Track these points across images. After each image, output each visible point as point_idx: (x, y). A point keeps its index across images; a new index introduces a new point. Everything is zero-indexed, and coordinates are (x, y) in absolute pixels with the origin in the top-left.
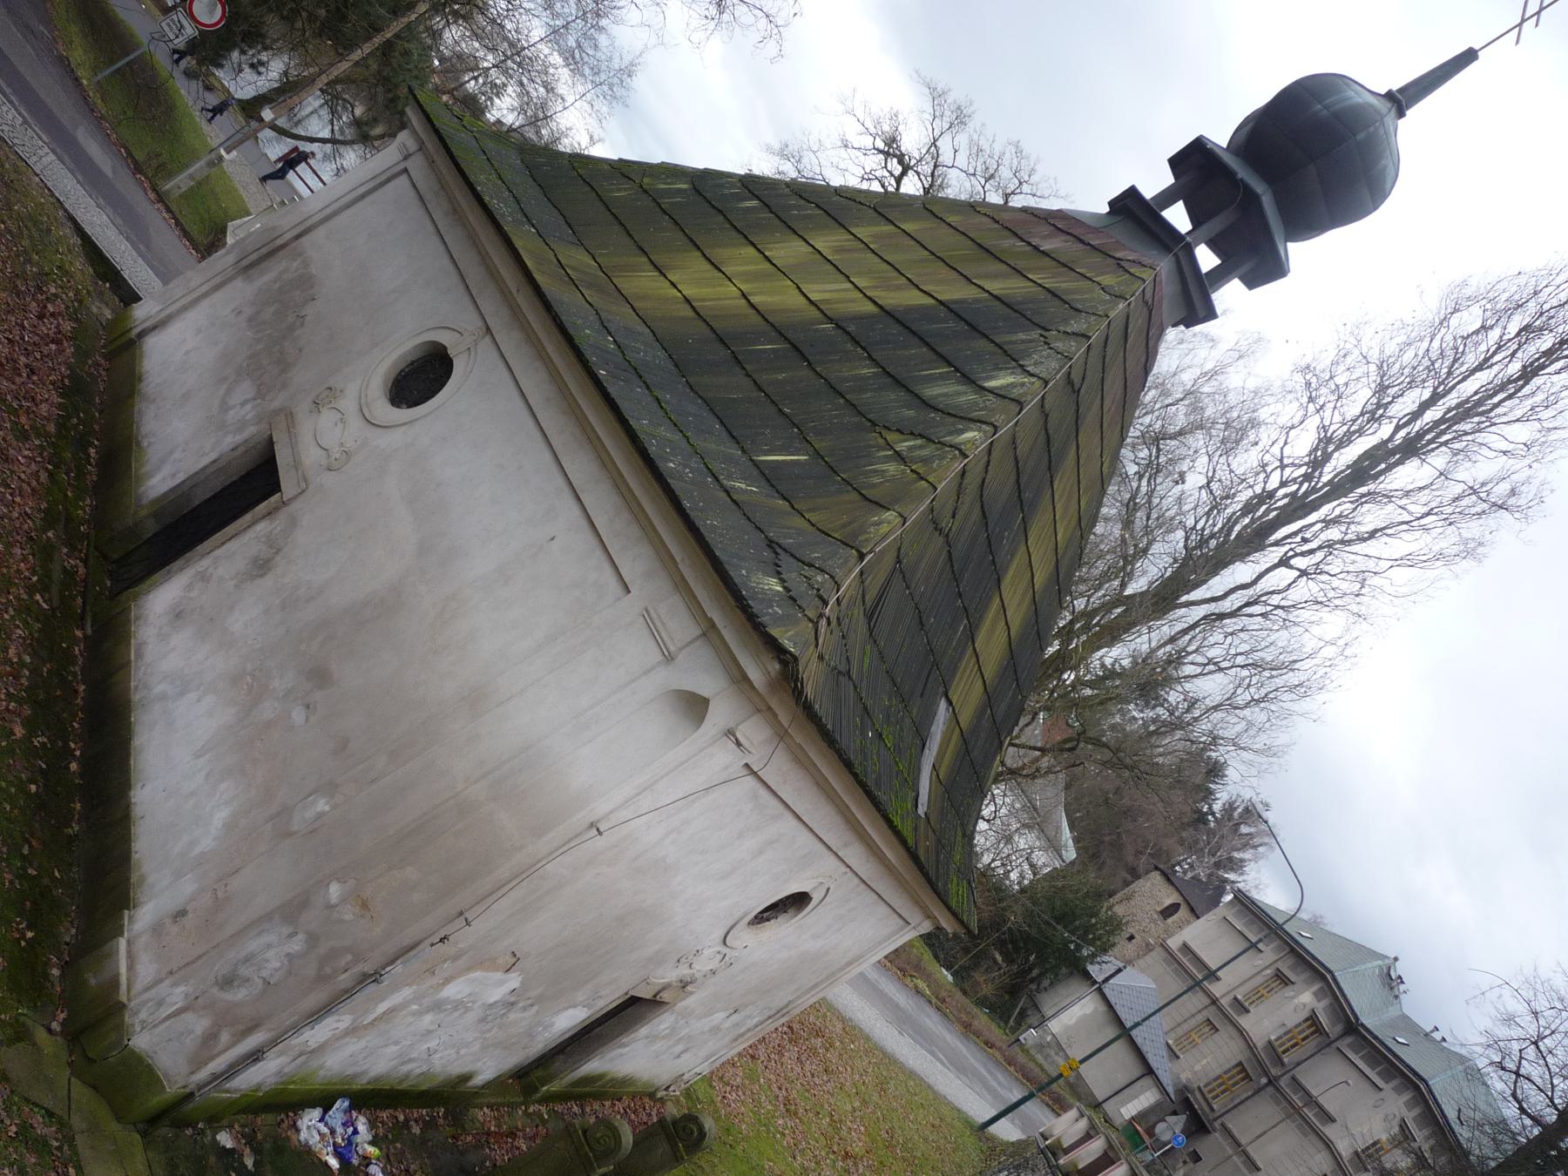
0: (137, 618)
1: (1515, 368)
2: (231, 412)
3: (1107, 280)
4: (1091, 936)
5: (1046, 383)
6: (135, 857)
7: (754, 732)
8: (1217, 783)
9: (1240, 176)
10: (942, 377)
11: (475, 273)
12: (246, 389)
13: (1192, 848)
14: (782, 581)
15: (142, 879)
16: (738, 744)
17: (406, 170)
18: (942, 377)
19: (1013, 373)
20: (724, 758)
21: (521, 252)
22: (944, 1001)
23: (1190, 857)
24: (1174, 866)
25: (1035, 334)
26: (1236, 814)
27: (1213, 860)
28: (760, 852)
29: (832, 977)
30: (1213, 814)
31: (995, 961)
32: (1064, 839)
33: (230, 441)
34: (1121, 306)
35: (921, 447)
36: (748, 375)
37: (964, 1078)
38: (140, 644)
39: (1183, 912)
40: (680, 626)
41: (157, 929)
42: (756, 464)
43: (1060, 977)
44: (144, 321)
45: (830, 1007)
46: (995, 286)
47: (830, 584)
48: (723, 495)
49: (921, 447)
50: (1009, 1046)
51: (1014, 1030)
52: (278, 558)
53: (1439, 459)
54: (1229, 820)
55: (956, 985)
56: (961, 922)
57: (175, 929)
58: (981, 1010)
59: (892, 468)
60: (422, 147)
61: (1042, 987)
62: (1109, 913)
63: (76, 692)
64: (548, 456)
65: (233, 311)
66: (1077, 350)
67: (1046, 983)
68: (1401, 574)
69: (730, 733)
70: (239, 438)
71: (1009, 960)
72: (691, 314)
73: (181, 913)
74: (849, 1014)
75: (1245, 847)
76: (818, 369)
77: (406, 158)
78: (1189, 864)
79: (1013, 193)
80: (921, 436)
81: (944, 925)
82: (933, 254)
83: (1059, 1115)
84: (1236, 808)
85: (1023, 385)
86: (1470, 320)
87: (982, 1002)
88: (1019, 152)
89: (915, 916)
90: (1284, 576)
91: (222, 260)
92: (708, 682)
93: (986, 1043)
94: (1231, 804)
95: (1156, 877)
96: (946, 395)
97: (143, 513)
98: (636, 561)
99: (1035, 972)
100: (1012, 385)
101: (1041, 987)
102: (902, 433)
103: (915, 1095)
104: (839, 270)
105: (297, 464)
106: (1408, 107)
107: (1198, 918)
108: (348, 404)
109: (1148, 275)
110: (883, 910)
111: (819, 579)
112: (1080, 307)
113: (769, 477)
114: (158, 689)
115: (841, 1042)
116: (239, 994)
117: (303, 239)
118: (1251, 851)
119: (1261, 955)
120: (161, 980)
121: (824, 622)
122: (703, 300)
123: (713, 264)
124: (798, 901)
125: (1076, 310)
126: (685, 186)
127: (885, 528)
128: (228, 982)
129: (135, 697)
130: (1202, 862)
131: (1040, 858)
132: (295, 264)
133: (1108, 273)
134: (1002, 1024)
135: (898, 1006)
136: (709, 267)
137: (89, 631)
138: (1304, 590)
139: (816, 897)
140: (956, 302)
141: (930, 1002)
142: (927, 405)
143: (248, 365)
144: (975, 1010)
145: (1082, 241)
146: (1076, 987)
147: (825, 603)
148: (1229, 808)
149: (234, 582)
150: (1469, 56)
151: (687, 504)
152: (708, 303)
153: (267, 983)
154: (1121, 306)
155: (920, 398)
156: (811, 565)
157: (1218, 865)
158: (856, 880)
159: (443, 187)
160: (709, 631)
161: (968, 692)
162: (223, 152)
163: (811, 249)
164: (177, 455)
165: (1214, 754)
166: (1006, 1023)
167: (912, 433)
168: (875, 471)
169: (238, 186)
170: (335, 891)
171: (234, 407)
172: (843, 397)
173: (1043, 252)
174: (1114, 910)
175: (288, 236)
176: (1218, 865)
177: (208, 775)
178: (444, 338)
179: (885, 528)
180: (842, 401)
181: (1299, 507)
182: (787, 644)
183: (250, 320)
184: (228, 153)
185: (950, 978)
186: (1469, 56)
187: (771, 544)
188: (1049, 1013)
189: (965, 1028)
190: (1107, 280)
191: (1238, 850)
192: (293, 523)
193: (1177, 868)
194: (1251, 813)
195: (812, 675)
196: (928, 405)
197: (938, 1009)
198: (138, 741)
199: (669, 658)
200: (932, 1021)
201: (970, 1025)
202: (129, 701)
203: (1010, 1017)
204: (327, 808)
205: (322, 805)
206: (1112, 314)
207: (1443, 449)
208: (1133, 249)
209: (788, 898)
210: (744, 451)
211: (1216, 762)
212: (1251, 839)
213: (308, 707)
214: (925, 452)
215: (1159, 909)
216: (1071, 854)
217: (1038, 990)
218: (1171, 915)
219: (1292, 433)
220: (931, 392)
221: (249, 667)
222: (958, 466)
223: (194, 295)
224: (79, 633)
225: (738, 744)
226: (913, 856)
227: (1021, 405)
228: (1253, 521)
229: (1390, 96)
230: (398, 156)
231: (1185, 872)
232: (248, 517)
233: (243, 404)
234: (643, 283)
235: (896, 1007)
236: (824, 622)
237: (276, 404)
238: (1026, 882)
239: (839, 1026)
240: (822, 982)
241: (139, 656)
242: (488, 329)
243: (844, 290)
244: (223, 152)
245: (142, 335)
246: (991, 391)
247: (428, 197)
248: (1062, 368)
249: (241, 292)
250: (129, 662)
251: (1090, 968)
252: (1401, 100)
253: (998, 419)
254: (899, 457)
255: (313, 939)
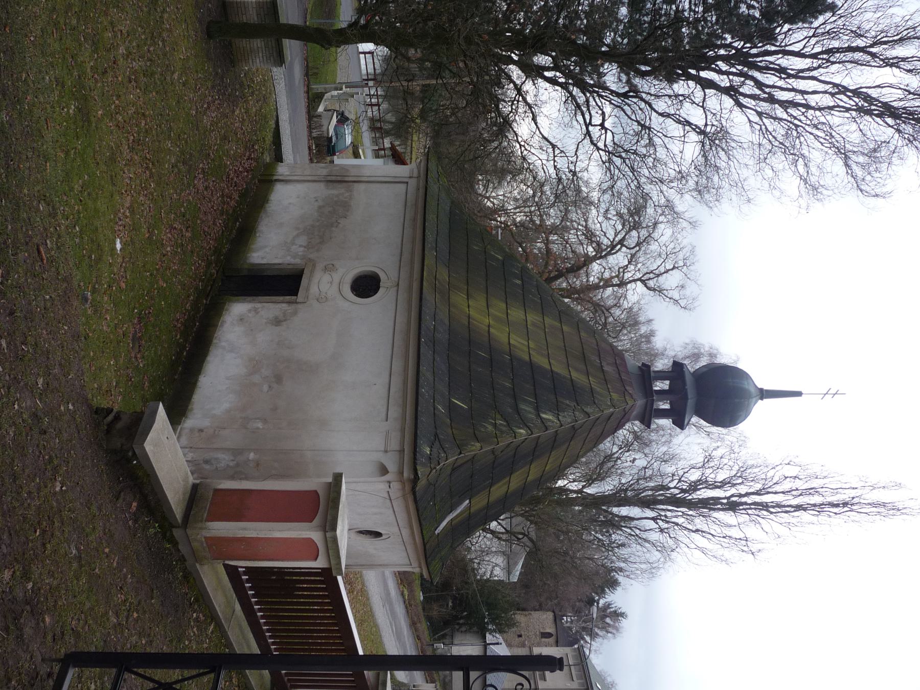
0: (227, 310)
1: (795, 502)
2: (294, 247)
3: (615, 396)
4: (497, 621)
5: (561, 426)
6: (193, 400)
7: (396, 486)
8: (610, 590)
9: (686, 387)
10: (530, 403)
11: (406, 256)
12: (303, 240)
13: (577, 612)
14: (431, 451)
15: (192, 410)
16: (390, 486)
17: (407, 183)
18: (530, 403)
19: (554, 416)
20: (383, 487)
21: (425, 267)
22: (411, 605)
23: (574, 617)
24: (564, 616)
25: (573, 404)
26: (609, 610)
27: (583, 625)
28: (376, 514)
29: (371, 566)
30: (598, 603)
31: (448, 605)
32: (516, 569)
33: (289, 259)
34: (611, 410)
35: (505, 426)
36: (469, 362)
37: (397, 643)
38: (223, 321)
39: (551, 640)
40: (394, 445)
41: (192, 430)
42: (450, 400)
43: (472, 630)
44: (281, 175)
45: (361, 576)
46: (574, 375)
47: (445, 459)
48: (432, 409)
49: (505, 426)
50: (427, 645)
51: (435, 640)
52: (284, 323)
53: (742, 518)
54: (603, 611)
55: (423, 603)
56: (431, 577)
57: (197, 435)
58: (426, 622)
59: (490, 428)
60: (418, 177)
61: (461, 630)
62: (513, 616)
63: (195, 325)
64: (390, 352)
65: (315, 198)
66: (581, 419)
67: (463, 629)
68: (697, 553)
69: (389, 482)
70: (293, 261)
71: (453, 608)
72: (467, 323)
73: (201, 430)
74: (367, 584)
75: (603, 628)
76: (493, 374)
77: (410, 177)
78: (571, 619)
79: (677, 268)
80: (507, 422)
81: (424, 574)
82: (565, 346)
83: (427, 683)
84: (610, 608)
85: (553, 422)
86: (791, 471)
87: (429, 619)
88: (692, 251)
89: (415, 564)
90: (651, 524)
91: (321, 169)
92: (392, 467)
93: (418, 636)
94: (609, 604)
95: (550, 615)
96: (525, 410)
97: (246, 266)
98: (395, 412)
99: (461, 621)
100: (549, 420)
101: (460, 630)
102: (502, 416)
103: (373, 635)
104: (528, 334)
105: (308, 289)
106: (765, 398)
107: (557, 646)
108: (336, 277)
109: (630, 403)
110: (405, 554)
111: (443, 455)
112: (596, 402)
113: (451, 407)
114: (223, 344)
115: (357, 594)
116: (207, 467)
117: (356, 184)
118: (604, 632)
119: (572, 682)
120: (187, 448)
121: (434, 471)
122: (474, 320)
123: (487, 304)
124: (377, 535)
125: (595, 403)
126: (500, 257)
127: (474, 448)
128: (207, 462)
129: (215, 341)
130: (578, 622)
131: (497, 571)
132: (347, 194)
133: (617, 393)
134: (432, 635)
135: (389, 594)
136: (485, 305)
137: (208, 303)
138: (654, 536)
139: (384, 537)
140: (557, 374)
141: (405, 602)
142: (518, 411)
143: (309, 229)
144: (423, 619)
145: (619, 374)
146: (476, 640)
147: (439, 464)
148: (608, 606)
149: (265, 321)
150: (798, 394)
151: (419, 409)
152: (475, 322)
153: (217, 468)
154: (611, 410)
155: (517, 407)
156: (443, 449)
157: (584, 629)
158: (401, 540)
159: (416, 204)
160: (402, 451)
161: (480, 502)
162: (344, 87)
163: (524, 318)
164: (267, 250)
165: (617, 576)
166: (434, 635)
167: (505, 419)
168: (485, 426)
169: (338, 68)
170: (252, 456)
171: (296, 245)
172: (494, 390)
173: (603, 370)
174: (516, 616)
175: (350, 179)
176: (584, 629)
177: (227, 388)
178: (382, 276)
179: (474, 448)
180: (492, 392)
181: (676, 502)
182: (419, 473)
183: (320, 207)
184: (346, 88)
185: (422, 598)
186: (798, 394)
187: (436, 435)
188: (456, 642)
189: (413, 624)
190: (615, 396)
191: (599, 628)
192: (295, 313)
193: (565, 618)
194: (618, 615)
195: (422, 483)
196: (518, 411)
197: (406, 607)
198: (209, 358)
199: (386, 451)
200: (400, 610)
201: (416, 624)
202: (212, 341)
203: (437, 633)
204: (261, 427)
205: (260, 425)
206: (605, 412)
207: (747, 516)
208: (634, 390)
209: (377, 532)
210: (449, 394)
211: (617, 580)
212: (608, 627)
213: (270, 387)
214: (504, 429)
215: (542, 631)
216: (515, 578)
217: (458, 630)
218: (546, 638)
219: (693, 470)
220: (523, 406)
221: (257, 358)
222: (511, 440)
223: (303, 178)
224: (204, 301)
225: (390, 486)
226: (424, 545)
227: (547, 429)
228: (652, 495)
229: (761, 390)
230: (407, 175)
231: (567, 622)
232: (281, 298)
233: (300, 246)
234: (459, 299)
235: (388, 594)
236: (434, 471)
237: (311, 256)
238: (485, 578)
239: (359, 587)
240: (367, 565)
241: (222, 326)
242: (398, 285)
243: (523, 344)
244: (344, 87)
245: (277, 180)
246: (541, 418)
247: (409, 204)
248: (571, 423)
249: (321, 190)
250: (217, 326)
251: (488, 635)
252: (765, 394)
253: (535, 431)
254: (495, 425)
255: (238, 465)
